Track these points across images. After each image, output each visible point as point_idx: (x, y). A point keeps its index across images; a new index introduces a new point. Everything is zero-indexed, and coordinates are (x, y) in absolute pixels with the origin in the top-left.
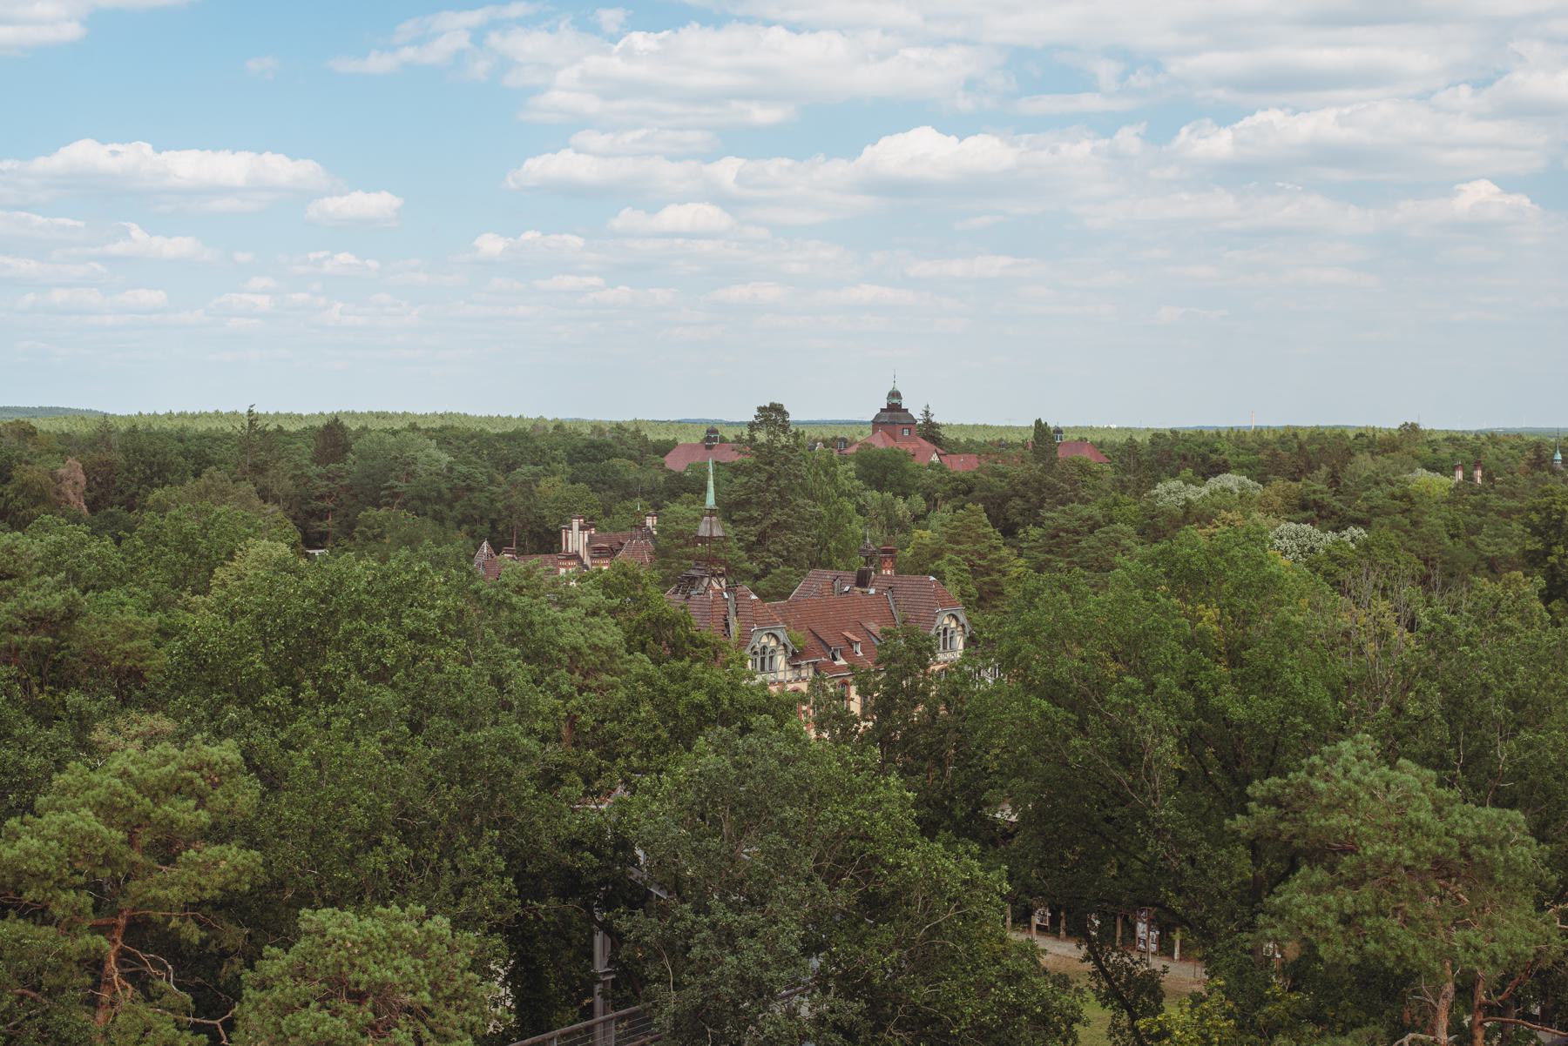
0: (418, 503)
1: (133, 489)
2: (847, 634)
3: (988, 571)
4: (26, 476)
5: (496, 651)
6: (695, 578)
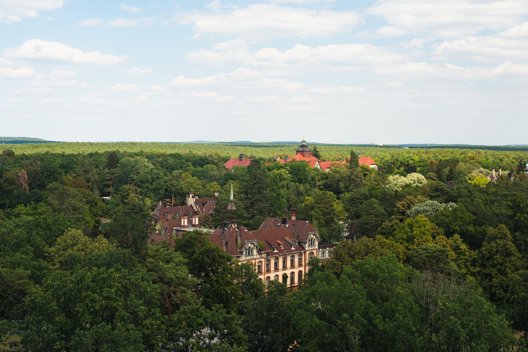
1: (44, 179)
2: (278, 241)
3: (329, 214)
4: (8, 176)
5: (134, 303)
6: (226, 224)
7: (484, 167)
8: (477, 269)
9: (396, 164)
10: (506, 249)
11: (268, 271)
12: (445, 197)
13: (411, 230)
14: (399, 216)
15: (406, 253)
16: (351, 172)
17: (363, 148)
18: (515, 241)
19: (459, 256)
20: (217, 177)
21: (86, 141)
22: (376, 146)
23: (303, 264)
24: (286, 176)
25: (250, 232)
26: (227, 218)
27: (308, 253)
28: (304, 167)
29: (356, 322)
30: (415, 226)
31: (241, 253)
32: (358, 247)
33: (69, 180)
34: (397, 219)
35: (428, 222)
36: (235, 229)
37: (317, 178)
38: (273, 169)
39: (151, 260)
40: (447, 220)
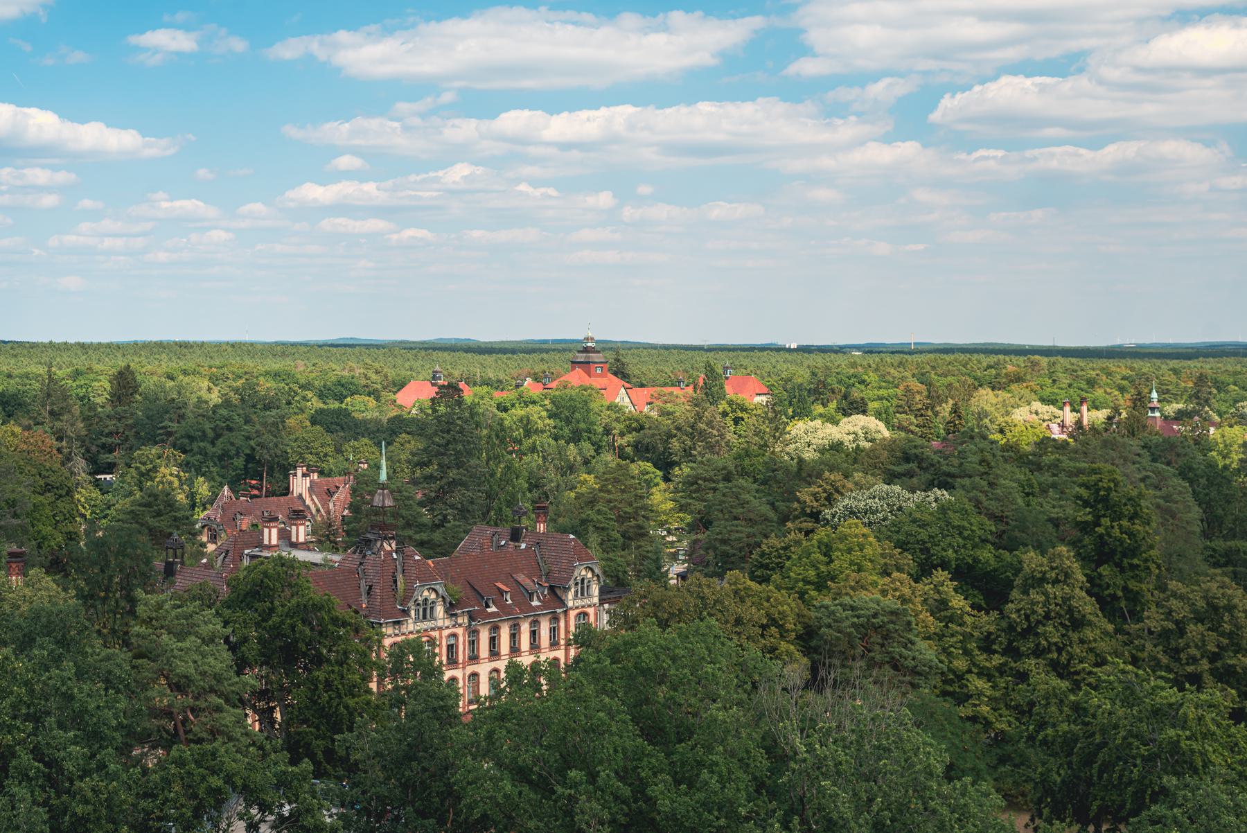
0: (186, 441)
2: (499, 585)
5: (54, 738)
7: (1043, 400)
8: (997, 660)
9: (821, 394)
10: (1070, 610)
11: (474, 658)
12: (927, 476)
13: (825, 559)
14: (805, 524)
15: (803, 616)
16: (698, 413)
17: (745, 354)
18: (1095, 588)
19: (946, 626)
20: (372, 426)
21: (71, 341)
22: (779, 349)
23: (562, 642)
24: (540, 424)
25: (430, 562)
26: (373, 527)
27: (573, 614)
28: (586, 402)
29: (602, 791)
30: (838, 549)
31: (406, 613)
32: (676, 601)
33: (13, 434)
34: (800, 530)
35: (871, 539)
36: (390, 553)
37: (618, 427)
38: (513, 405)
39: (143, 630)
40: (923, 535)
